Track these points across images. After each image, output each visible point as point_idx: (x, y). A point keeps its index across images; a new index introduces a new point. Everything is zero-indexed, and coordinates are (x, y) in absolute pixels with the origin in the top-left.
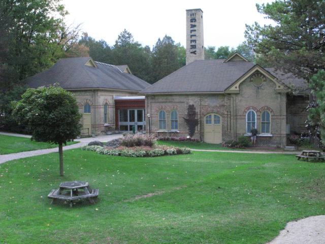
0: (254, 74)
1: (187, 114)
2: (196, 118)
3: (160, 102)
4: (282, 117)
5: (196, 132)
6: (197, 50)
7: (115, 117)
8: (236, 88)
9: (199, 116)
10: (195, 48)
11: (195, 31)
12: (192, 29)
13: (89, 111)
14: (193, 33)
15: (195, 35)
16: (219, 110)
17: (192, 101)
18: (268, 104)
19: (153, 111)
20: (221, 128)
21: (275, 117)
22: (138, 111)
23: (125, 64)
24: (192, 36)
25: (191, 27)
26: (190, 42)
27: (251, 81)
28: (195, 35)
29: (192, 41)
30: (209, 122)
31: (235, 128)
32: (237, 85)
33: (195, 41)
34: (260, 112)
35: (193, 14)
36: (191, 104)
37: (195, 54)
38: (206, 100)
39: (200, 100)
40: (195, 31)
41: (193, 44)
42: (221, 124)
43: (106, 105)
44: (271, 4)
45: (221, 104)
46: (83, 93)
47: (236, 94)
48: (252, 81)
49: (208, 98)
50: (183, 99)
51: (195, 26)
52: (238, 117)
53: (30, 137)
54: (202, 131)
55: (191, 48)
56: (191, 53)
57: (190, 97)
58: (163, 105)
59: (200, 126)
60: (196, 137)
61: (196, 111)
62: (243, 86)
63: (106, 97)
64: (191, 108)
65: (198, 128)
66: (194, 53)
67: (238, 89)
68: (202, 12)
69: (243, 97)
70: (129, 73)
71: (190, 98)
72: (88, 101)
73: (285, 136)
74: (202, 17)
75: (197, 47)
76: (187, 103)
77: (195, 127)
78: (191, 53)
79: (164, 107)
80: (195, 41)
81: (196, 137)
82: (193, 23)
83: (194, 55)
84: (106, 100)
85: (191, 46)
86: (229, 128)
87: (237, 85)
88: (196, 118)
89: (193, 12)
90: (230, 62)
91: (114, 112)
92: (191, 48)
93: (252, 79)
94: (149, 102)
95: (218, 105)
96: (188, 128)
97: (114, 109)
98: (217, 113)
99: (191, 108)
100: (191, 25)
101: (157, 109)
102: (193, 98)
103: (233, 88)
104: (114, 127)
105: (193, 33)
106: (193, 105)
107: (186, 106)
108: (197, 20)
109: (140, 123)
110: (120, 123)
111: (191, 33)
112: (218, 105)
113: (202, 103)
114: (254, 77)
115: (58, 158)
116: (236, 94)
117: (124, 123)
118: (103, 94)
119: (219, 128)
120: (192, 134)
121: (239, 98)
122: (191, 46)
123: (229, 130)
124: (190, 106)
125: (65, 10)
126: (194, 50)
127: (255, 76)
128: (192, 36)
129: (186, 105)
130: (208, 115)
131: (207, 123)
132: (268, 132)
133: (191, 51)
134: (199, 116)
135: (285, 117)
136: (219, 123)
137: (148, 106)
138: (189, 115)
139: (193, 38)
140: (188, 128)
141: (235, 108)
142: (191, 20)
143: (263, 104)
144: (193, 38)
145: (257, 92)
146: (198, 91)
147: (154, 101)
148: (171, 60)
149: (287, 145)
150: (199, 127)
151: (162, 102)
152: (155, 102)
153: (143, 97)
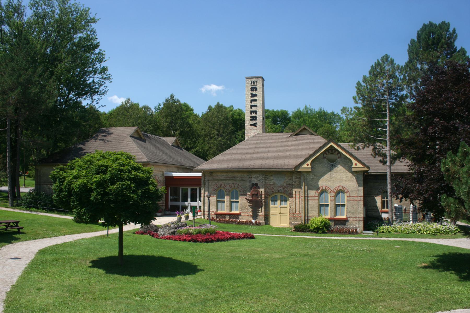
0: (327, 150)
3: (218, 180)
5: (260, 214)
11: (256, 100)
12: (252, 98)
14: (253, 103)
15: (255, 106)
16: (286, 189)
21: (351, 198)
22: (192, 190)
25: (251, 97)
26: (250, 113)
28: (255, 106)
32: (309, 162)
35: (254, 82)
37: (256, 126)
38: (272, 178)
39: (265, 178)
40: (256, 100)
41: (253, 115)
44: (458, 45)
45: (288, 183)
48: (325, 158)
51: (255, 95)
56: (251, 125)
59: (265, 208)
60: (261, 219)
66: (255, 125)
67: (310, 166)
69: (315, 176)
71: (254, 176)
76: (250, 182)
78: (251, 125)
79: (223, 186)
80: (255, 112)
82: (254, 93)
83: (254, 127)
85: (251, 117)
86: (297, 210)
87: (309, 162)
93: (325, 155)
94: (206, 179)
95: (285, 184)
98: (284, 193)
100: (251, 94)
101: (215, 188)
102: (257, 175)
103: (305, 166)
104: (164, 207)
105: (253, 103)
109: (194, 204)
110: (170, 203)
111: (251, 102)
112: (285, 184)
113: (267, 181)
114: (327, 153)
115: (116, 241)
120: (255, 216)
122: (251, 117)
123: (297, 213)
125: (108, 73)
126: (254, 122)
127: (329, 152)
129: (248, 184)
130: (274, 195)
131: (201, 206)
135: (362, 198)
137: (205, 184)
142: (251, 88)
146: (263, 167)
148: (299, 118)
149: (364, 230)
153: (200, 174)
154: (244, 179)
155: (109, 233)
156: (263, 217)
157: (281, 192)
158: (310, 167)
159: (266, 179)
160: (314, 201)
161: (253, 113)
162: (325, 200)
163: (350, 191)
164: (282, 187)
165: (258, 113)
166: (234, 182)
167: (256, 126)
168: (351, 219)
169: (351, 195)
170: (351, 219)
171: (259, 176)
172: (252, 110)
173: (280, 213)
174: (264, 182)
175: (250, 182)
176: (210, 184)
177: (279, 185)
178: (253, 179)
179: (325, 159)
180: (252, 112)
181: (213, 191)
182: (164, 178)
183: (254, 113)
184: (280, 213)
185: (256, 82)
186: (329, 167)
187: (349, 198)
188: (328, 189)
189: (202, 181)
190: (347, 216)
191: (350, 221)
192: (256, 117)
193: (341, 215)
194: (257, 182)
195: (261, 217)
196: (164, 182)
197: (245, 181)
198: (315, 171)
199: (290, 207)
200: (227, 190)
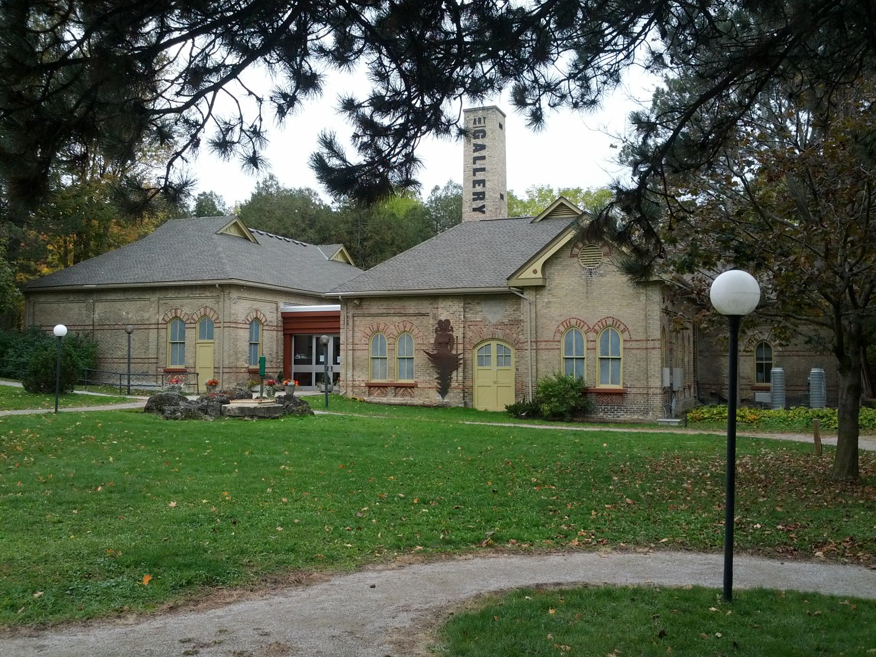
1: (432, 341)
2: (454, 352)
4: (651, 344)
5: (454, 384)
6: (487, 202)
7: (281, 353)
8: (535, 272)
9: (461, 347)
10: (483, 198)
12: (477, 154)
13: (211, 337)
15: (483, 170)
17: (447, 311)
18: (615, 312)
19: (358, 335)
20: (514, 376)
21: (634, 345)
23: (339, 243)
24: (475, 171)
25: (475, 151)
26: (471, 185)
27: (573, 256)
28: (483, 170)
29: (475, 183)
30: (483, 360)
31: (534, 371)
32: (538, 265)
33: (482, 182)
34: (597, 333)
35: (480, 119)
36: (443, 318)
37: (484, 212)
38: (478, 308)
39: (464, 308)
40: (483, 158)
41: (479, 189)
42: (512, 367)
43: (256, 322)
46: (197, 294)
47: (538, 288)
48: (576, 256)
49: (483, 305)
50: (425, 307)
51: (483, 147)
52: (543, 345)
53: (19, 385)
54: (468, 383)
55: (474, 200)
56: (474, 210)
57: (440, 301)
58: (381, 320)
61: (455, 335)
62: (550, 271)
63: (257, 305)
64: (444, 327)
65: (457, 377)
66: (481, 209)
67: (539, 275)
68: (504, 116)
70: (349, 263)
71: (442, 304)
72: (208, 310)
73: (659, 391)
74: (501, 126)
75: (486, 196)
76: (435, 317)
77: (451, 373)
78: (474, 210)
79: (381, 327)
80: (482, 182)
81: (454, 398)
84: (257, 311)
85: (474, 194)
87: (538, 265)
88: (454, 352)
89: (480, 114)
90: (545, 222)
91: (281, 342)
92: (474, 200)
93: (576, 250)
95: (506, 321)
96: (436, 376)
97: (281, 334)
99: (444, 327)
102: (448, 303)
103: (528, 274)
106: (448, 321)
107: (430, 323)
108: (488, 133)
110: (295, 368)
111: (474, 163)
116: (538, 288)
117: (303, 369)
118: (245, 295)
119: (508, 377)
120: (443, 390)
121: (544, 298)
122: (474, 194)
124: (440, 323)
126: (480, 203)
128: (475, 171)
129: (431, 321)
131: (480, 364)
132: (618, 383)
133: (475, 206)
134: (461, 347)
135: (657, 344)
136: (508, 363)
138: (438, 344)
139: (480, 176)
140: (436, 376)
141: (534, 324)
143: (603, 312)
144: (480, 176)
145: (588, 284)
147: (359, 312)
150: (461, 374)
151: (381, 315)
152: (364, 316)
154: (423, 312)
155: (719, 559)
156: (459, 391)
157: (498, 339)
158: (541, 276)
159: (467, 310)
160: (552, 352)
161: (477, 185)
162: (577, 350)
163: (630, 328)
164: (500, 327)
165: (487, 184)
166: (404, 318)
167: (484, 212)
168: (634, 391)
169: (634, 338)
170: (634, 391)
171: (451, 304)
172: (476, 178)
173: (495, 382)
174: (462, 317)
175: (435, 317)
176: (357, 323)
177: (494, 321)
178: (440, 311)
179: (576, 259)
180: (475, 183)
181: (363, 338)
182: (280, 315)
183: (479, 185)
184: (495, 382)
185: (484, 118)
186: (583, 277)
187: (628, 345)
188: (582, 324)
189: (342, 318)
190: (624, 384)
191: (630, 397)
192: (483, 193)
193: (612, 383)
194: (448, 318)
195: (455, 391)
196: (280, 324)
197: (423, 315)
198: (552, 286)
199: (517, 370)
200: (391, 335)
